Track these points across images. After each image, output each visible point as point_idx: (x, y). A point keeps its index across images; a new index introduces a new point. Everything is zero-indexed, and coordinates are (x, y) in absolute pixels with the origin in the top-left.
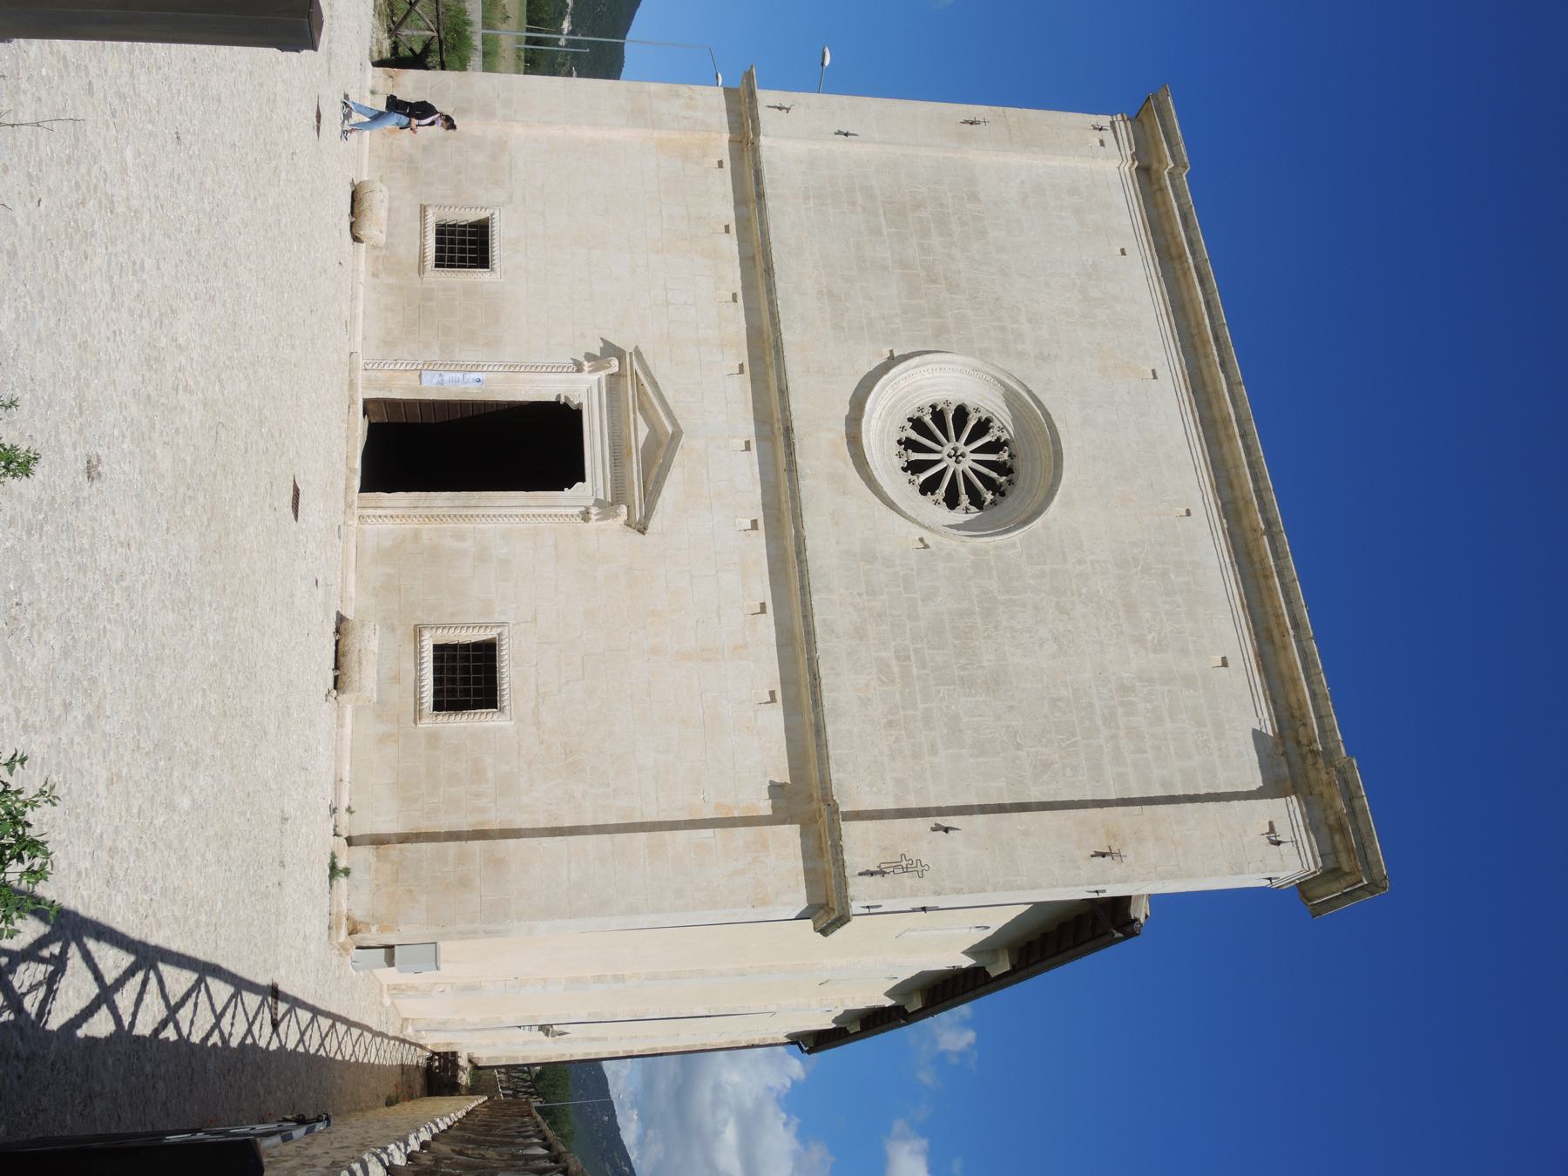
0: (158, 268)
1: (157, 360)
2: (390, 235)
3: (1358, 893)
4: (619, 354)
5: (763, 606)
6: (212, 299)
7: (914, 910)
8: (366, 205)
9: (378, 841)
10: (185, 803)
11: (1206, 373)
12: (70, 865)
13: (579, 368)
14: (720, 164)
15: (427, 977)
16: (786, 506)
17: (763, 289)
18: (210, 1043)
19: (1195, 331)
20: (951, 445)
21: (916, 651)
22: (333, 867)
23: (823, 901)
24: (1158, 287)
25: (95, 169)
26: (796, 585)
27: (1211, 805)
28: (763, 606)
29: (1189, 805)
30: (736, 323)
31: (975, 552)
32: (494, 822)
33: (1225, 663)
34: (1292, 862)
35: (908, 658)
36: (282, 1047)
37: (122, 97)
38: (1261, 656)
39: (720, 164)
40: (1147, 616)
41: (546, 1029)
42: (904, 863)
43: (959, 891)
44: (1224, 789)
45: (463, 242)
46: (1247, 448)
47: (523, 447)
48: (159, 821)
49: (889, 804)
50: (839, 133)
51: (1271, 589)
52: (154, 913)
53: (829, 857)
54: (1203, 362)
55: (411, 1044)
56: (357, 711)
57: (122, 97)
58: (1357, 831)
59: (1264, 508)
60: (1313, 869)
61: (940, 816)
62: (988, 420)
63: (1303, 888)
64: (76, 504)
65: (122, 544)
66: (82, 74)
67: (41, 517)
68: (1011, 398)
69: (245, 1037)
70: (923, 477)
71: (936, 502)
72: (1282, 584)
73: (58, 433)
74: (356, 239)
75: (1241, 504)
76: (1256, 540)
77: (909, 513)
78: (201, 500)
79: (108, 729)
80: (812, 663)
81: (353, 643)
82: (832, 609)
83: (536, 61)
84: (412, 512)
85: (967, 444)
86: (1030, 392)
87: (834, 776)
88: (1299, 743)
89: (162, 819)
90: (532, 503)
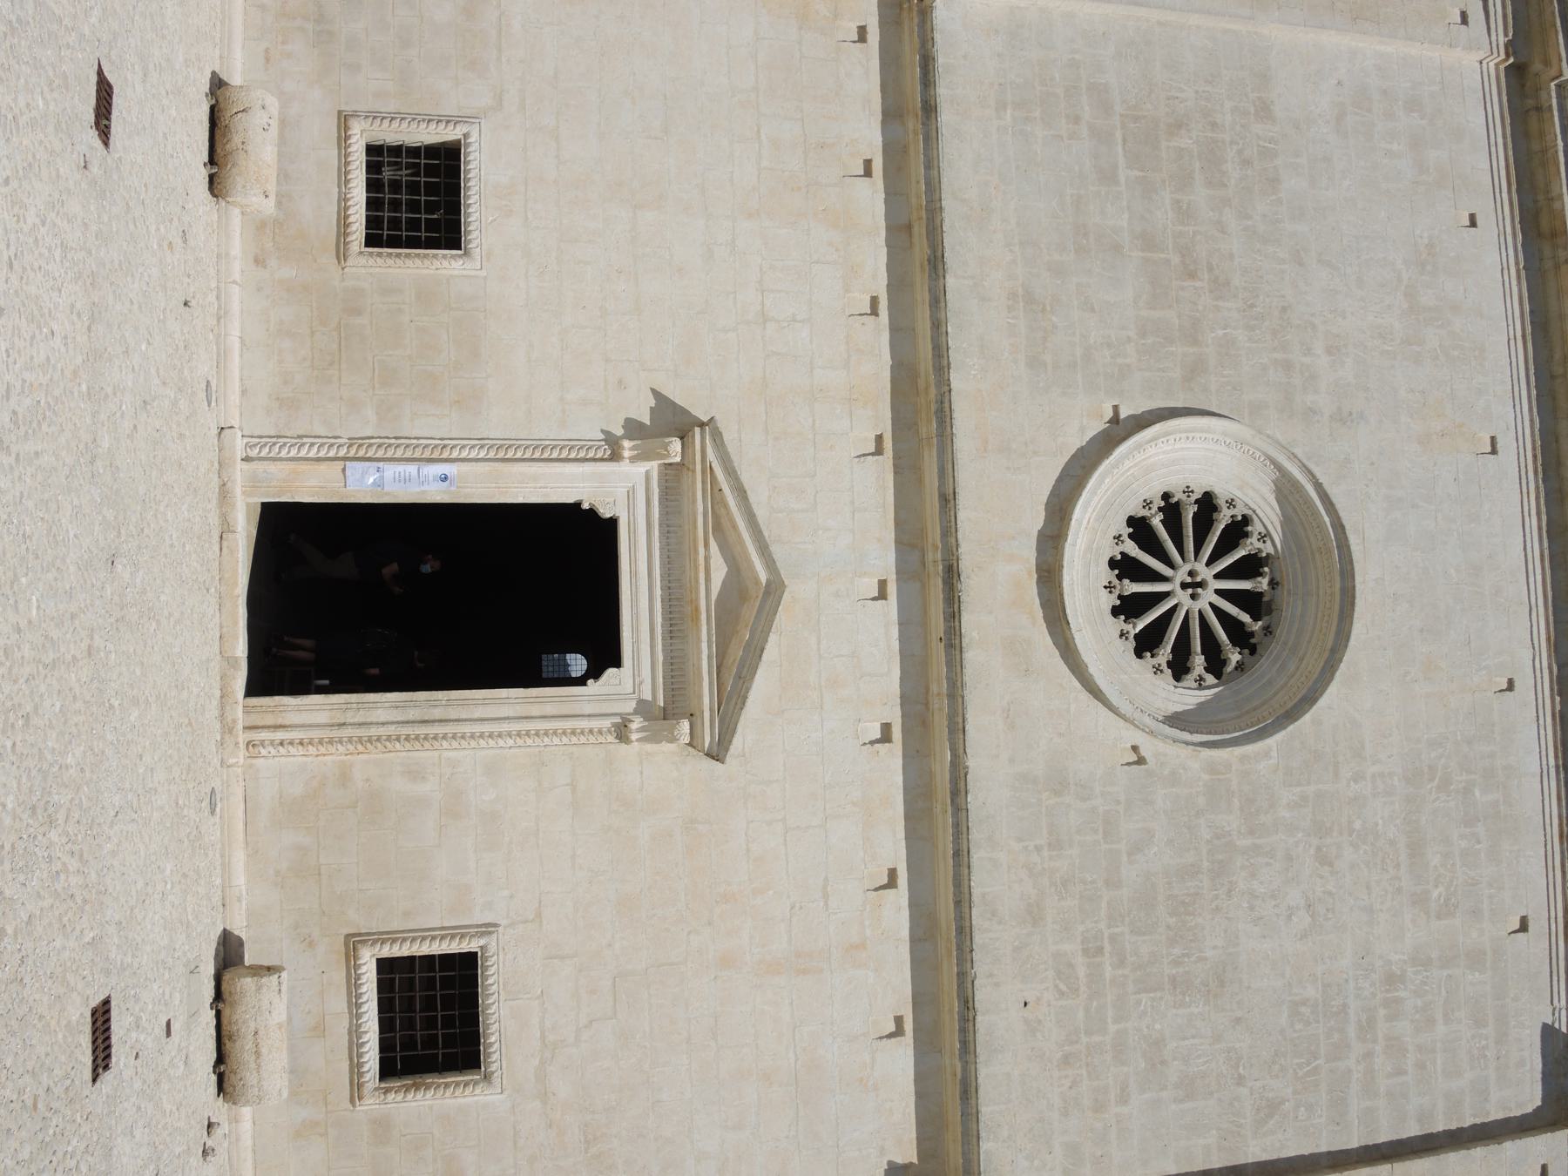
8: (236, 140)
16: (940, 705)
17: (922, 295)
20: (1187, 567)
21: (1112, 938)
24: (1516, 288)
28: (892, 873)
30: (872, 356)
35: (1100, 950)
40: (1436, 860)
62: (1246, 520)
68: (1286, 490)
80: (964, 981)
82: (997, 878)
84: (336, 733)
85: (1209, 563)
86: (1318, 486)
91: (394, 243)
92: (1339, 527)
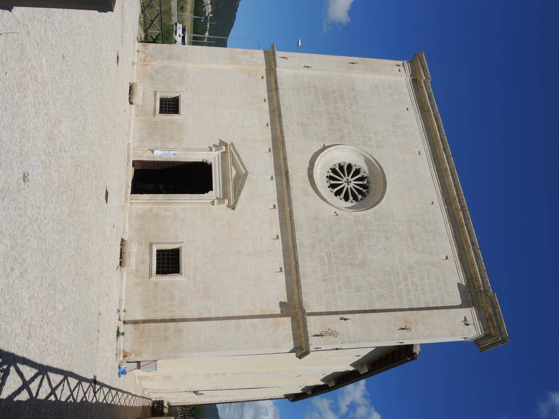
0: (55, 105)
1: (53, 139)
2: (143, 102)
3: (497, 343)
4: (226, 145)
5: (277, 236)
6: (76, 119)
7: (333, 349)
8: (135, 91)
9: (135, 322)
10: (60, 307)
11: (438, 152)
12: (12, 331)
13: (211, 150)
14: (262, 77)
15: (152, 373)
16: (286, 200)
17: (278, 122)
18: (69, 401)
19: (434, 138)
20: (346, 178)
21: (334, 253)
22: (118, 332)
23: (300, 346)
24: (420, 122)
25: (30, 64)
26: (289, 229)
27: (443, 311)
28: (277, 236)
29: (435, 311)
31: (355, 217)
32: (178, 316)
33: (447, 258)
34: (473, 332)
35: (331, 256)
36: (97, 402)
37: (42, 39)
38: (460, 256)
39: (262, 77)
41: (196, 392)
42: (330, 332)
43: (350, 342)
44: (448, 304)
45: (169, 104)
46: (454, 179)
47: (191, 178)
48: (50, 314)
49: (324, 310)
50: (305, 67)
51: (463, 231)
52: (47, 350)
53: (302, 329)
54: (437, 149)
55: (146, 398)
56: (128, 274)
57: (42, 39)
58: (497, 320)
59: (460, 201)
60: (481, 334)
61: (343, 314)
62: (359, 169)
63: (477, 342)
64: (19, 190)
65: (37, 207)
66: (25, 27)
67: (3, 194)
68: (368, 161)
69: (83, 398)
70: (336, 190)
71: (341, 199)
72: (467, 229)
73: (11, 163)
74: (131, 103)
75: (452, 200)
76: (458, 213)
77: (331, 202)
78: (70, 193)
79: (29, 278)
80: (296, 257)
81: (127, 249)
83: (196, 41)
85: (352, 178)
86: (374, 159)
87: (304, 299)
88: (475, 288)
89: (51, 313)
90: (194, 198)
91: (165, 113)
92: (381, 167)
